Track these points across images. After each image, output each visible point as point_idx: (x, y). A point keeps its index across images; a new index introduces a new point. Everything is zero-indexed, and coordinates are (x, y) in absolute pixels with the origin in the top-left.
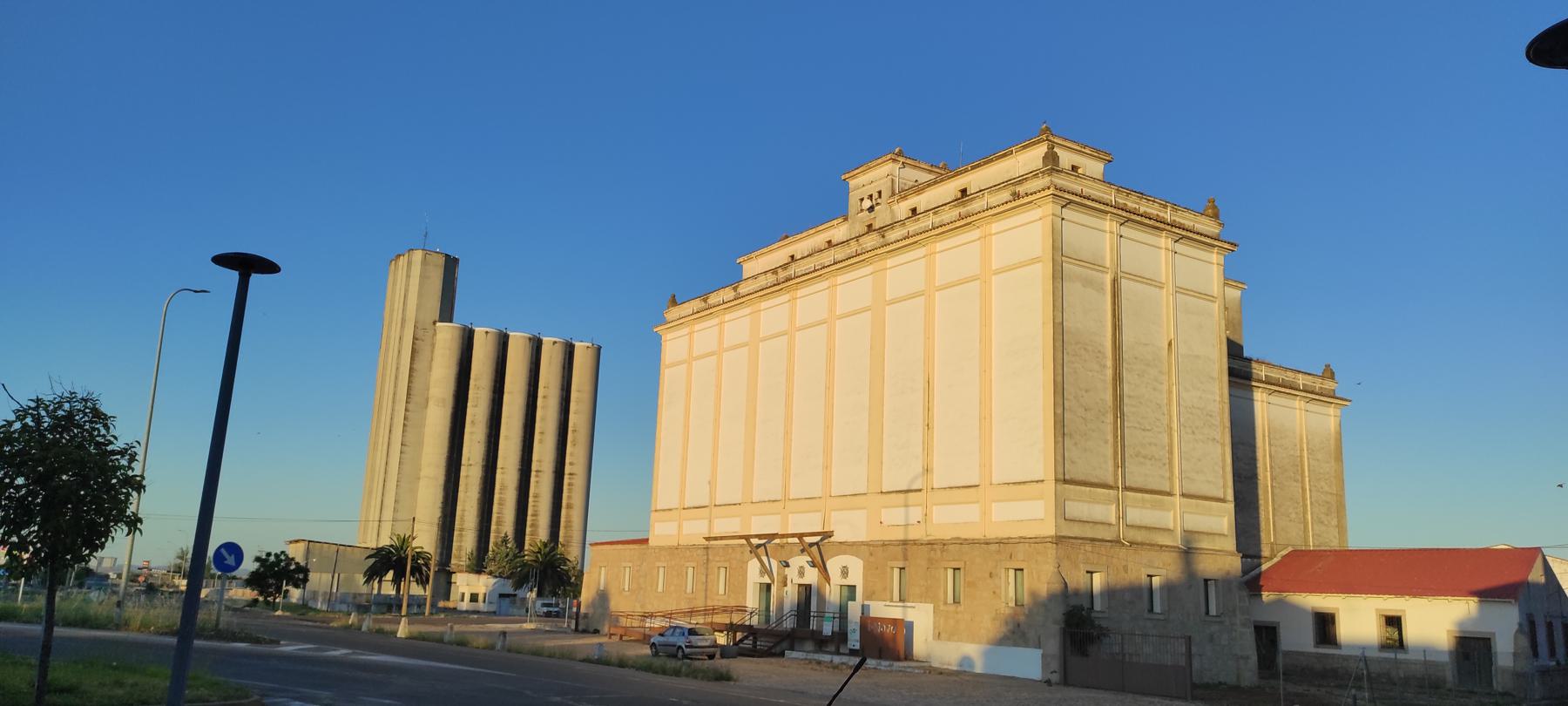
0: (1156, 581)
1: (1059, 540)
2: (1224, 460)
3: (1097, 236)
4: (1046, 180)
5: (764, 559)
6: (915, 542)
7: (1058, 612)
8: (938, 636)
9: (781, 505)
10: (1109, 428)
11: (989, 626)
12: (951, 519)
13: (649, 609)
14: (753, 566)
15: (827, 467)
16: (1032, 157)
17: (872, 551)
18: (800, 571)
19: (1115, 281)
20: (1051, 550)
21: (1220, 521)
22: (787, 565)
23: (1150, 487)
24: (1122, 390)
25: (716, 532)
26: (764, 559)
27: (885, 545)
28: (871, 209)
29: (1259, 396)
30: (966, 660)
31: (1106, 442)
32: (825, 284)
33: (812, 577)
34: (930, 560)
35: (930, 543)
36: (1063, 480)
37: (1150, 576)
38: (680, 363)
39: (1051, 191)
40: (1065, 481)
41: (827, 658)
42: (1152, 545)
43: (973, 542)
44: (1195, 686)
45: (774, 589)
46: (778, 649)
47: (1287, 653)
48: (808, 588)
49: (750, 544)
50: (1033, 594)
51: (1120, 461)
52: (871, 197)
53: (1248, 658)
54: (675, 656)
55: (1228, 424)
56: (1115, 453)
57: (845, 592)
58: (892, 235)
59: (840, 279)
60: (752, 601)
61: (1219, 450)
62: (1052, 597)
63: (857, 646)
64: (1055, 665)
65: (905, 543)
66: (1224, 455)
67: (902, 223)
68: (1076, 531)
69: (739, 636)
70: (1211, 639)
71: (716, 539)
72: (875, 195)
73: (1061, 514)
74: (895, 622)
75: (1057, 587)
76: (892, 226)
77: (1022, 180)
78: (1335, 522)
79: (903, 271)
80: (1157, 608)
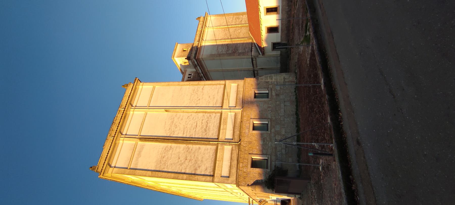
2: (210, 85)
42: (241, 127)
47: (281, 40)
61: (207, 86)
66: (208, 85)
78: (241, 16)
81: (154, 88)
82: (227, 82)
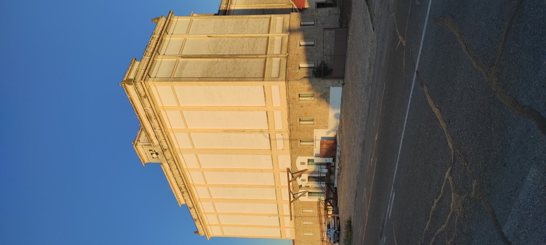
0: (302, 43)
1: (287, 80)
2: (255, 18)
3: (163, 64)
4: (139, 84)
5: (299, 195)
6: (290, 136)
7: (316, 80)
8: (326, 127)
9: (277, 188)
10: (242, 60)
11: (322, 107)
12: (280, 122)
13: (319, 239)
14: (302, 199)
15: (262, 171)
16: (131, 88)
17: (294, 153)
18: (303, 181)
19: (183, 57)
20: (291, 83)
21: (278, 19)
22: (301, 186)
23: (266, 45)
24: (227, 55)
25: (289, 214)
26: (299, 195)
27: (291, 148)
28: (157, 154)
29: (232, 8)
30: (336, 116)
31: (248, 61)
32: (187, 173)
33: (305, 176)
34: (297, 130)
35: (290, 130)
36: (263, 78)
37: (300, 45)
38: (222, 230)
39: (143, 82)
40: (264, 77)
41: (337, 171)
43: (289, 114)
44: (341, 26)
45: (310, 191)
46: (334, 190)
48: (309, 177)
49: (293, 201)
50: (309, 90)
51: (256, 56)
52: (152, 154)
53: (329, 11)
54: (339, 234)
55: (241, 16)
56: (252, 58)
57: (310, 163)
58: (165, 146)
59: (185, 167)
60: (315, 199)
61: (251, 19)
62: (310, 82)
63: (332, 159)
64: (336, 82)
65: (290, 140)
66: (253, 18)
67: (160, 142)
68: (283, 73)
69: (329, 204)
70: (323, 24)
71: (291, 213)
72: (151, 152)
73: (276, 79)
74: (322, 144)
75: (306, 81)
76: (161, 146)
77: (139, 94)
79: (180, 142)
80: (312, 43)
81: (191, 21)
82: (272, 15)
